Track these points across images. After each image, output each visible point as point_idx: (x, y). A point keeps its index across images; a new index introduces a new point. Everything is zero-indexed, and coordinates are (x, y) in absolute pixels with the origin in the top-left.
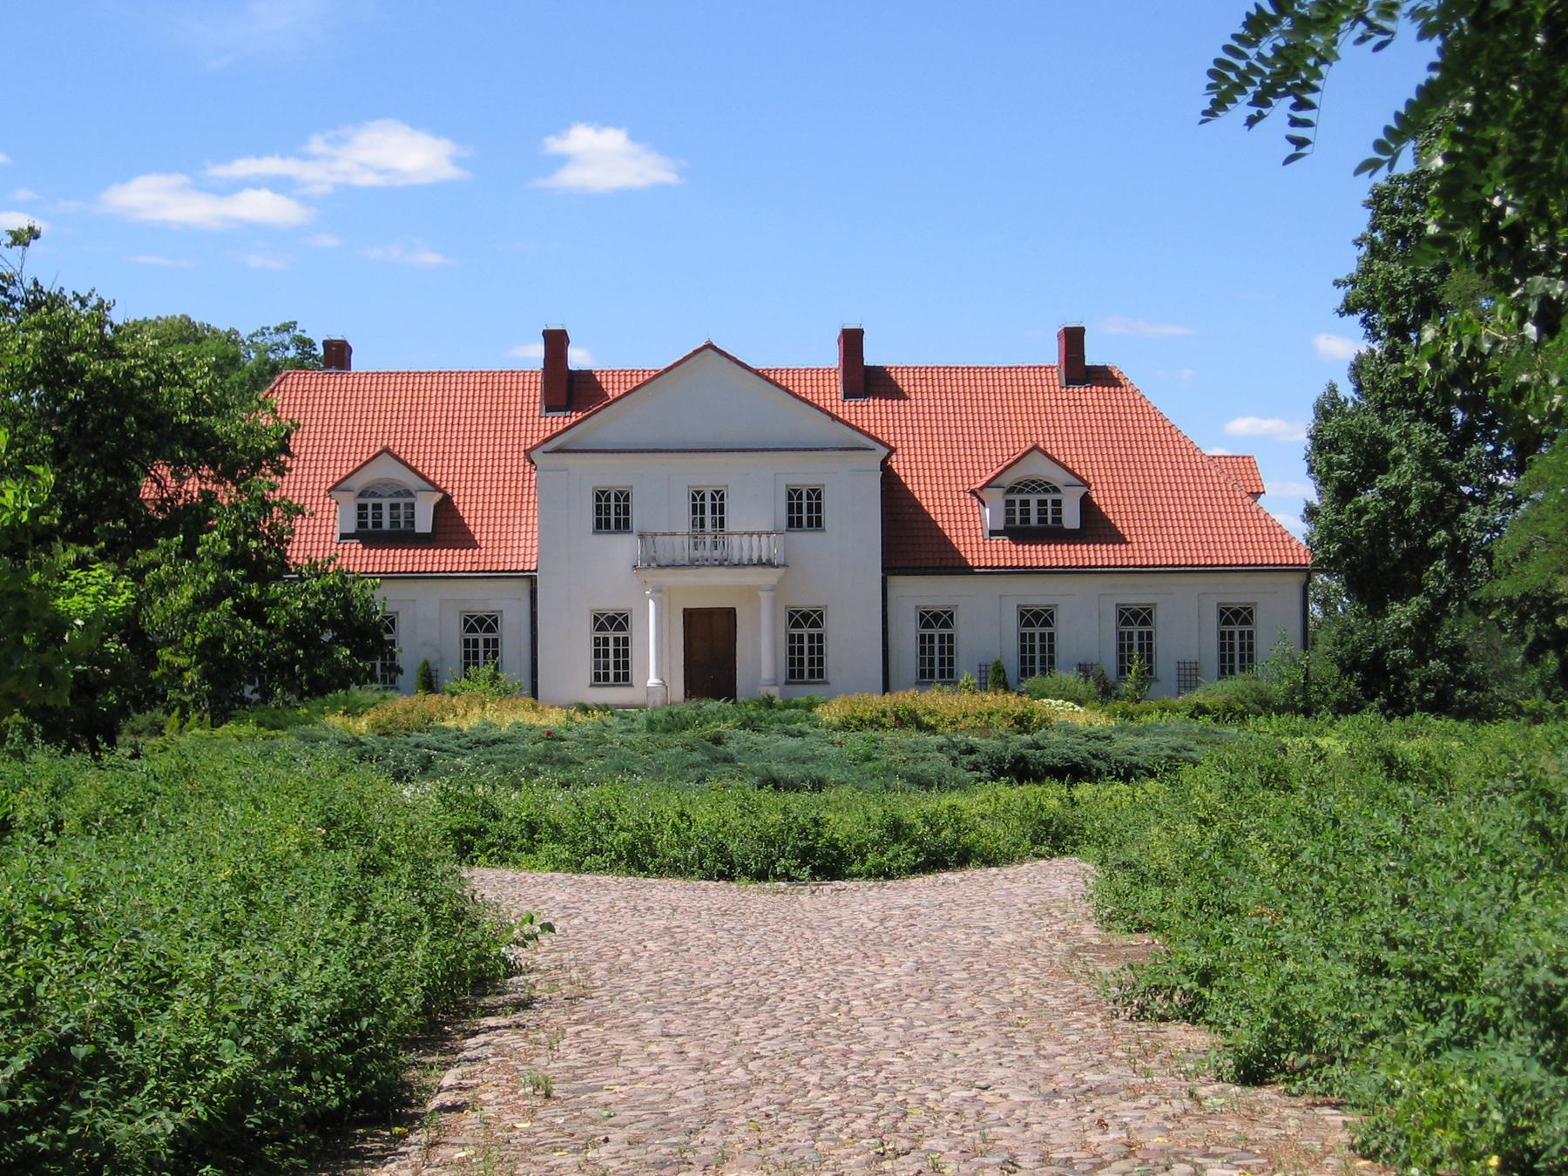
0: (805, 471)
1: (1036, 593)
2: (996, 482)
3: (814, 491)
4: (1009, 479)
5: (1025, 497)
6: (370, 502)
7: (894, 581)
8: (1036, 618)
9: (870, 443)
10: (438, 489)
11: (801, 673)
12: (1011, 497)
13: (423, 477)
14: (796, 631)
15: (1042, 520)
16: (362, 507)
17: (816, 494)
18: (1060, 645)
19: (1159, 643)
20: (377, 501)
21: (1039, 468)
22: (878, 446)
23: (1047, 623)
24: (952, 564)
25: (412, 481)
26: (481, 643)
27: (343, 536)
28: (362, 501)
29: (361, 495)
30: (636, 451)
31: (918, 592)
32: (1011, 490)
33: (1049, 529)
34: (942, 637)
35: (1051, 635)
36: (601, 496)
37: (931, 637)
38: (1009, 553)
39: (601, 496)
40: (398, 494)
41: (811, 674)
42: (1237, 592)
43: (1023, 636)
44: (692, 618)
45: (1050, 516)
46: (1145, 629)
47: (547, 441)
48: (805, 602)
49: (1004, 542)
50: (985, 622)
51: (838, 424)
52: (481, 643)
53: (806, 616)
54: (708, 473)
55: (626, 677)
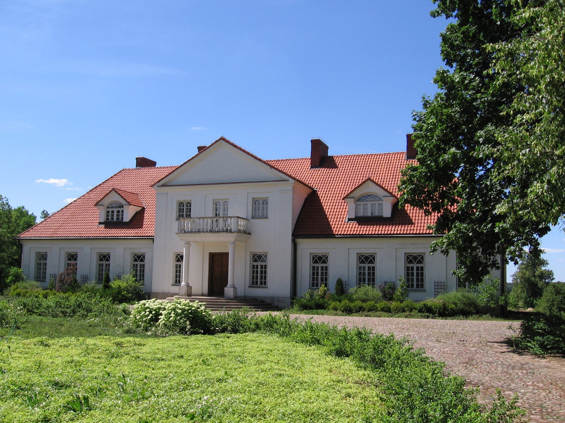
0: (259, 191)
1: (366, 247)
2: (351, 195)
3: (189, 203)
4: (357, 194)
5: (112, 209)
6: (110, 210)
7: (300, 241)
8: (367, 259)
9: (286, 178)
10: (394, 196)
11: (412, 286)
12: (108, 210)
13: (386, 190)
14: (255, 264)
15: (118, 219)
16: (108, 212)
17: (189, 204)
18: (377, 273)
19: (426, 272)
20: (112, 209)
21: (371, 188)
22: (290, 179)
23: (324, 262)
24: (326, 232)
25: (123, 202)
26: (367, 268)
27: (349, 220)
28: (108, 210)
29: (108, 207)
30: (238, 183)
31: (310, 247)
32: (359, 200)
33: (110, 222)
34: (262, 266)
35: (374, 268)
36: (181, 204)
37: (40, 263)
38: (355, 228)
39: (181, 204)
40: (120, 207)
41: (418, 286)
42: (72, 248)
43: (408, 268)
44: (213, 256)
45: (110, 218)
46: (420, 265)
47: (158, 182)
48: (259, 250)
49: (354, 224)
50: (342, 261)
51: (273, 170)
52: (139, 266)
53: (367, 258)
54: (220, 193)
55: (422, 286)
